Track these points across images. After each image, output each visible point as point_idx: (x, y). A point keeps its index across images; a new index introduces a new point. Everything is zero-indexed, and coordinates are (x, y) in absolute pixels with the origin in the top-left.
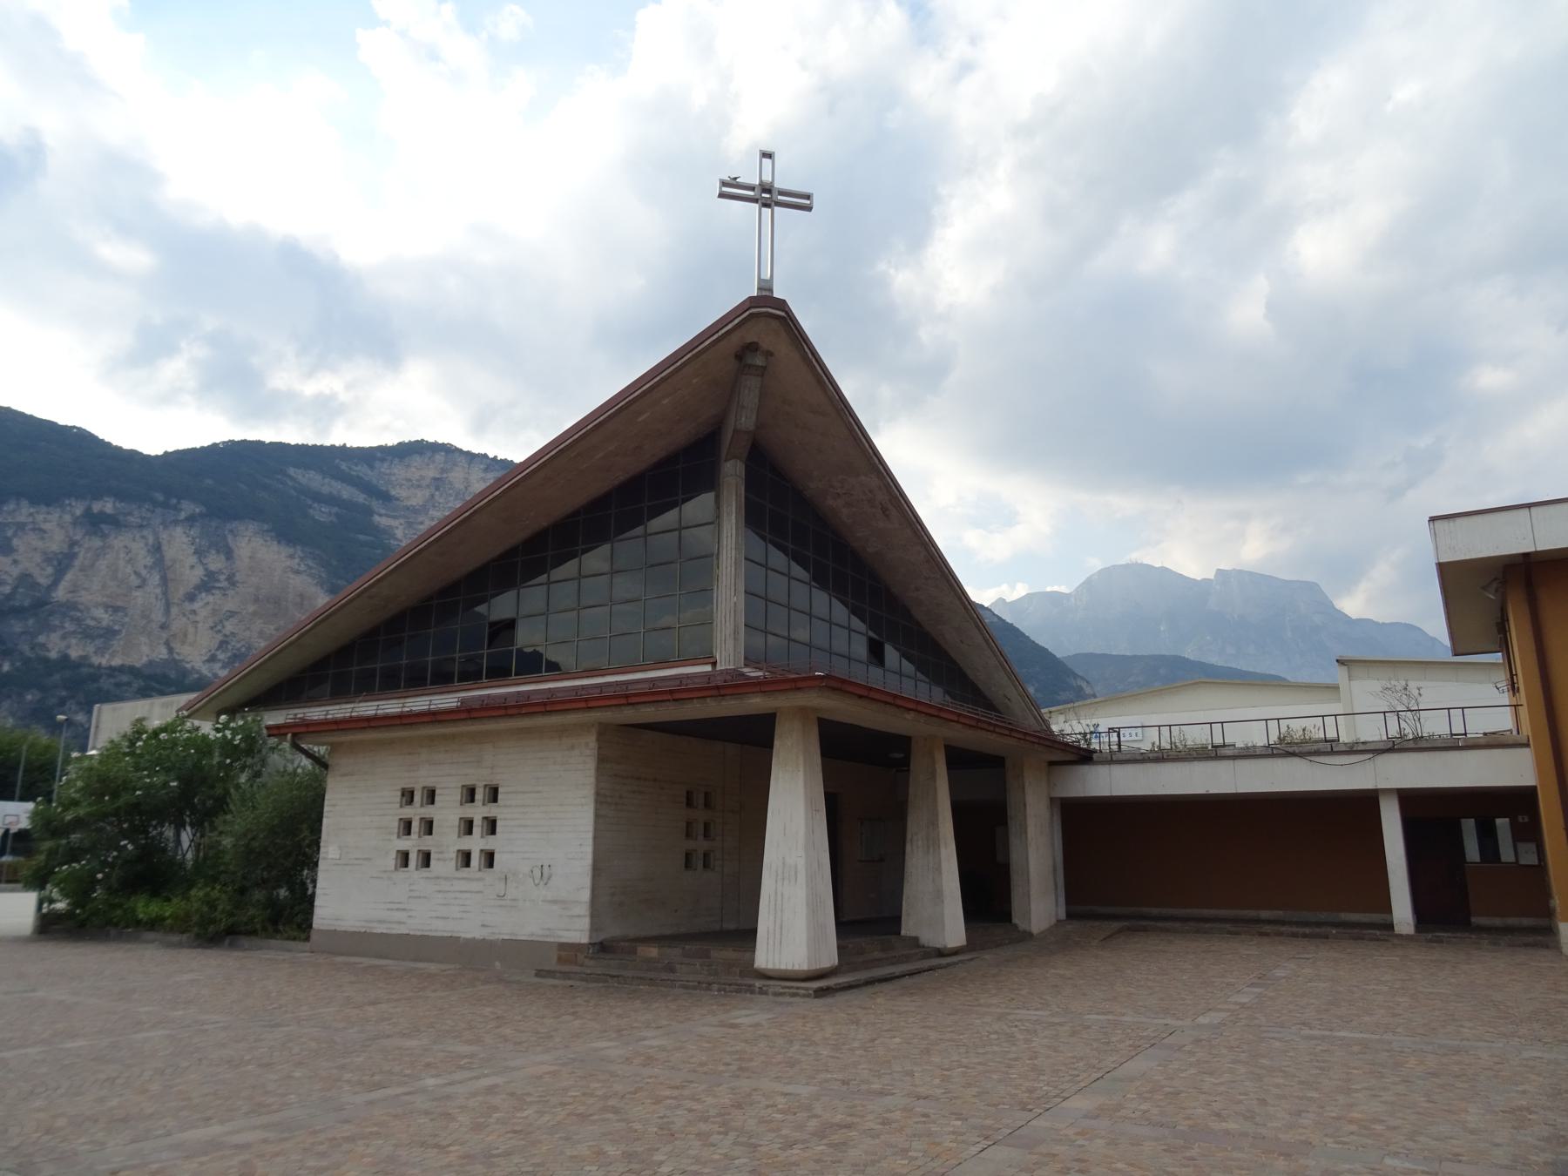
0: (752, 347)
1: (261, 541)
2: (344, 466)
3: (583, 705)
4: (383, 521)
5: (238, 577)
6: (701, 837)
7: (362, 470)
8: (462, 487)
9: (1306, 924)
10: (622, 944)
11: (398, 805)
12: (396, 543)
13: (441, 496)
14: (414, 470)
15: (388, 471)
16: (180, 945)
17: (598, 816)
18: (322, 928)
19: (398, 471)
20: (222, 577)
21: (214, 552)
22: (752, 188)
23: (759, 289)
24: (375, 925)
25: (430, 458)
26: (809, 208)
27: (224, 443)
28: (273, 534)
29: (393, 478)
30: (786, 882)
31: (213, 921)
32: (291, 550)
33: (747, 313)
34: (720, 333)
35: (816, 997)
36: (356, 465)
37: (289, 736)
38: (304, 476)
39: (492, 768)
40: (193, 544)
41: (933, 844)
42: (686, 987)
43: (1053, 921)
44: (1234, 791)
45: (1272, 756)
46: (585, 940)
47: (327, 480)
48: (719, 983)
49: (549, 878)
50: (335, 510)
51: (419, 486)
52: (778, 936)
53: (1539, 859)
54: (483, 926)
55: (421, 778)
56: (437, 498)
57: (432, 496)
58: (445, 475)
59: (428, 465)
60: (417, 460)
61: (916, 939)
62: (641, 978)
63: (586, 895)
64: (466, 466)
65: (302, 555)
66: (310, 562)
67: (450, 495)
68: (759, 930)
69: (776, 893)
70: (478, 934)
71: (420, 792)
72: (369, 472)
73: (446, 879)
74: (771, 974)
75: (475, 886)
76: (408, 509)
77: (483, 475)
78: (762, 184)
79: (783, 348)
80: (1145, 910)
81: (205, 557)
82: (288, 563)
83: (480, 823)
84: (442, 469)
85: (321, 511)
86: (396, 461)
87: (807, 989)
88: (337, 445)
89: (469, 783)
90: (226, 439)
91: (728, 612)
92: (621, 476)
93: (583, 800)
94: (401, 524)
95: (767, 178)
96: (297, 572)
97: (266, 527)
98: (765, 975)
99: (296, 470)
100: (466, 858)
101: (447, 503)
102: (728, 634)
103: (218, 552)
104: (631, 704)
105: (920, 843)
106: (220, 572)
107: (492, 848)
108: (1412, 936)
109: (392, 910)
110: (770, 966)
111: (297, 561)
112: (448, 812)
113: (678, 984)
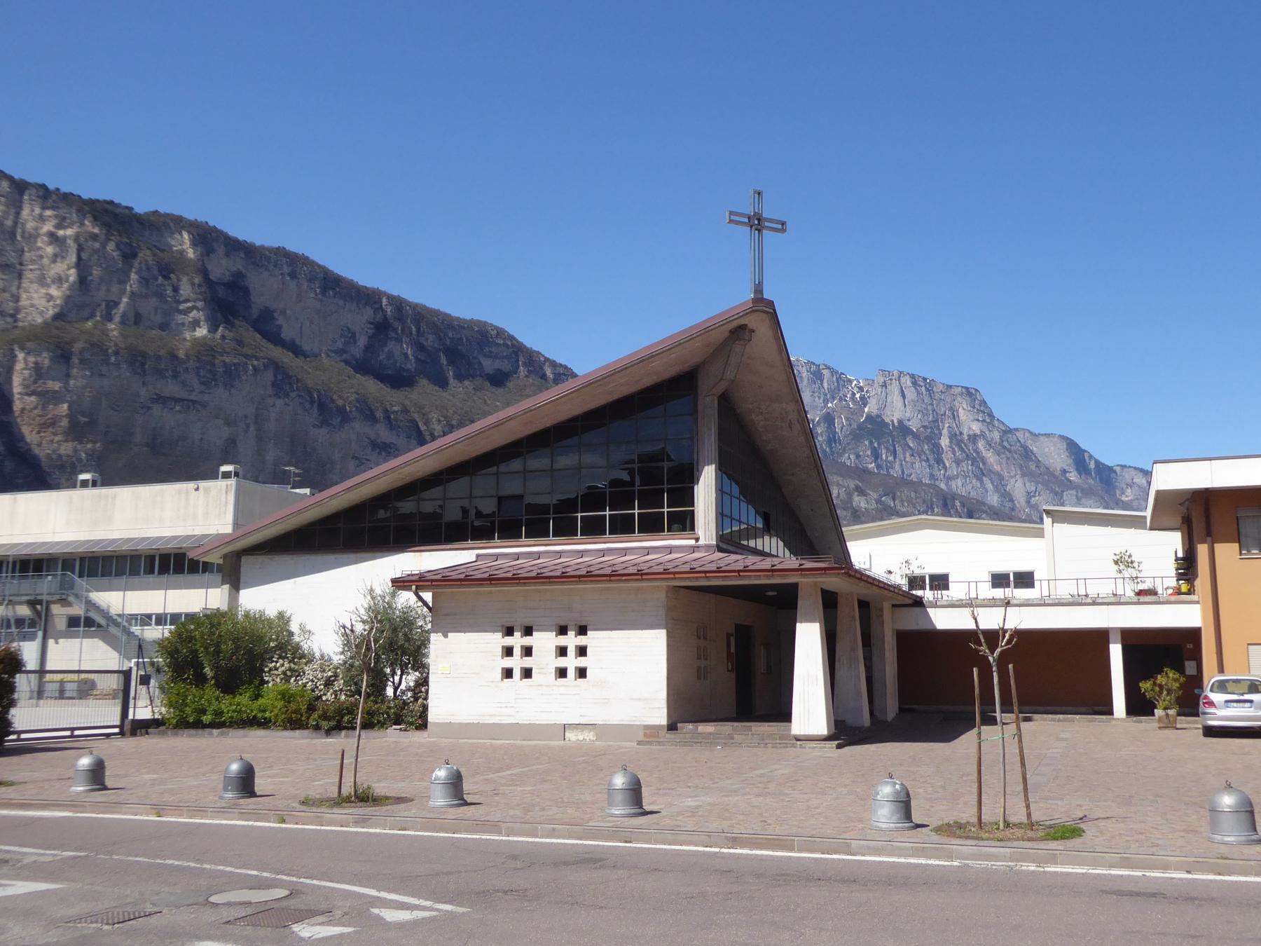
0: (743, 327)
37: (414, 587)
45: (1045, 605)
48: (772, 744)
53: (1198, 672)
54: (581, 716)
73: (547, 686)
74: (801, 738)
91: (710, 505)
98: (797, 739)
100: (562, 673)
102: (710, 520)
105: (845, 662)
107: (584, 666)
108: (1124, 719)
109: (501, 707)
110: (802, 733)
113: (743, 745)
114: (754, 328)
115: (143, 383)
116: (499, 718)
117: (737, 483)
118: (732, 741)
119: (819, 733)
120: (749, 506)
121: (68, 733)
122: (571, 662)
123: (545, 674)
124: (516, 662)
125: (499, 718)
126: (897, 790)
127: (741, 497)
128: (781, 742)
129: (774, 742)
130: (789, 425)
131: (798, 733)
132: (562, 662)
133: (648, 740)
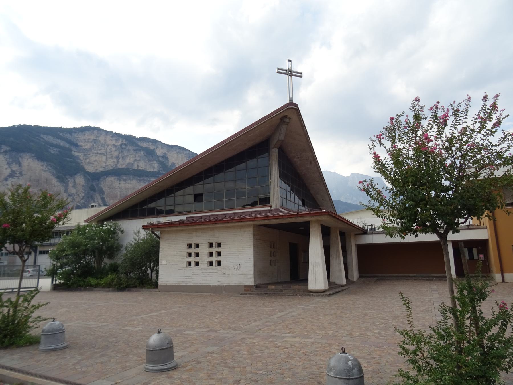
0: (286, 117)
1: (32, 160)
2: (61, 134)
3: (254, 219)
4: (76, 154)
5: (23, 173)
6: (273, 256)
7: (68, 136)
8: (104, 142)
9: (428, 277)
10: (263, 285)
11: (186, 249)
12: (80, 161)
13: (96, 145)
14: (86, 136)
15: (77, 136)
16: (109, 291)
17: (254, 250)
18: (162, 284)
19: (81, 137)
20: (17, 173)
21: (14, 163)
22: (286, 71)
23: (290, 100)
24: (181, 283)
25: (92, 132)
26: (301, 77)
27: (17, 125)
28: (36, 158)
29: (79, 139)
30: (316, 267)
31: (122, 284)
32: (43, 163)
33: (287, 108)
34: (278, 113)
35: (329, 296)
36: (66, 134)
37: (151, 229)
38: (47, 138)
39: (218, 237)
40: (6, 161)
41: (338, 257)
42: (289, 295)
43: (357, 278)
44: (408, 241)
46: (253, 284)
47: (55, 139)
48: (299, 294)
49: (240, 268)
50: (58, 149)
51: (88, 142)
52: (315, 281)
54: (218, 282)
55: (193, 241)
56: (95, 146)
57: (93, 145)
58: (97, 138)
59: (91, 134)
60: (87, 133)
61: (335, 282)
62: (275, 294)
63: (252, 272)
64: (105, 135)
65: (46, 165)
66: (49, 168)
67: (100, 145)
68: (309, 279)
69: (313, 270)
70: (217, 284)
71: (193, 245)
72: (70, 136)
74: (313, 291)
75: (215, 271)
76: (84, 149)
77: (111, 138)
78: (289, 69)
79: (294, 118)
80: (377, 275)
81: (11, 165)
82: (42, 168)
83: (215, 253)
84: (96, 136)
85: (54, 150)
86: (80, 133)
87: (326, 294)
88: (59, 127)
89: (211, 242)
90: (18, 124)
92: (238, 151)
93: (249, 246)
94: (82, 155)
95: (290, 68)
96: (45, 171)
97: (33, 155)
98: (311, 291)
99: (44, 135)
100: (211, 263)
101: (98, 148)
103: (16, 164)
104: (269, 219)
105: (334, 257)
106: (17, 171)
109: (186, 278)
110: (313, 289)
111: (45, 167)
112: (204, 250)
113: (286, 295)
114: (291, 117)
115: (140, 185)
116: (186, 283)
117: (289, 186)
118: (282, 293)
119: (321, 289)
120: (296, 196)
121: (10, 291)
122: (214, 259)
123: (204, 264)
124: (192, 259)
125: (186, 283)
126: (349, 366)
127: (291, 192)
128: (303, 293)
129: (301, 293)
130: (310, 163)
131: (311, 289)
132: (211, 259)
133: (246, 292)
